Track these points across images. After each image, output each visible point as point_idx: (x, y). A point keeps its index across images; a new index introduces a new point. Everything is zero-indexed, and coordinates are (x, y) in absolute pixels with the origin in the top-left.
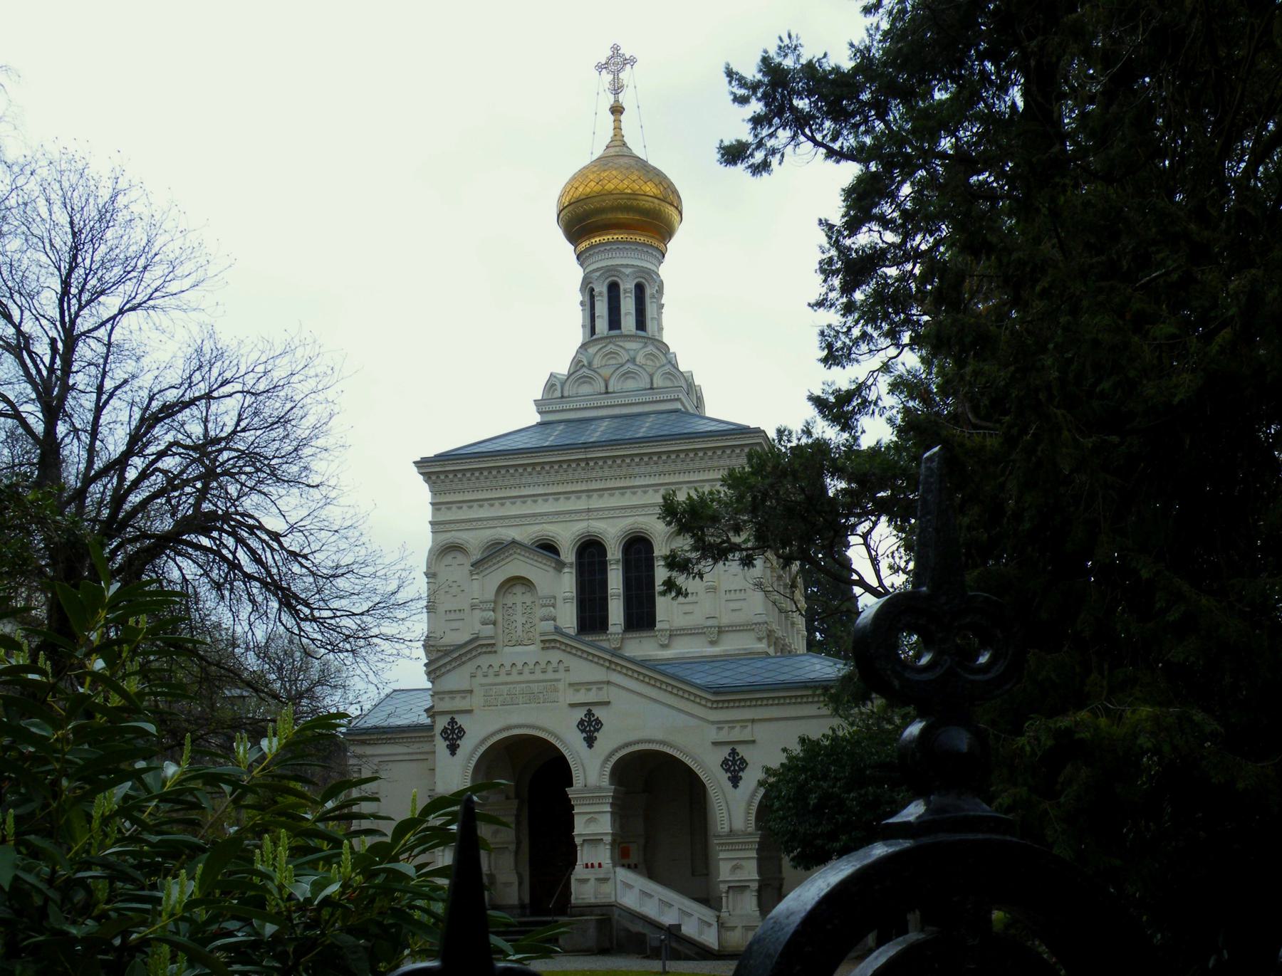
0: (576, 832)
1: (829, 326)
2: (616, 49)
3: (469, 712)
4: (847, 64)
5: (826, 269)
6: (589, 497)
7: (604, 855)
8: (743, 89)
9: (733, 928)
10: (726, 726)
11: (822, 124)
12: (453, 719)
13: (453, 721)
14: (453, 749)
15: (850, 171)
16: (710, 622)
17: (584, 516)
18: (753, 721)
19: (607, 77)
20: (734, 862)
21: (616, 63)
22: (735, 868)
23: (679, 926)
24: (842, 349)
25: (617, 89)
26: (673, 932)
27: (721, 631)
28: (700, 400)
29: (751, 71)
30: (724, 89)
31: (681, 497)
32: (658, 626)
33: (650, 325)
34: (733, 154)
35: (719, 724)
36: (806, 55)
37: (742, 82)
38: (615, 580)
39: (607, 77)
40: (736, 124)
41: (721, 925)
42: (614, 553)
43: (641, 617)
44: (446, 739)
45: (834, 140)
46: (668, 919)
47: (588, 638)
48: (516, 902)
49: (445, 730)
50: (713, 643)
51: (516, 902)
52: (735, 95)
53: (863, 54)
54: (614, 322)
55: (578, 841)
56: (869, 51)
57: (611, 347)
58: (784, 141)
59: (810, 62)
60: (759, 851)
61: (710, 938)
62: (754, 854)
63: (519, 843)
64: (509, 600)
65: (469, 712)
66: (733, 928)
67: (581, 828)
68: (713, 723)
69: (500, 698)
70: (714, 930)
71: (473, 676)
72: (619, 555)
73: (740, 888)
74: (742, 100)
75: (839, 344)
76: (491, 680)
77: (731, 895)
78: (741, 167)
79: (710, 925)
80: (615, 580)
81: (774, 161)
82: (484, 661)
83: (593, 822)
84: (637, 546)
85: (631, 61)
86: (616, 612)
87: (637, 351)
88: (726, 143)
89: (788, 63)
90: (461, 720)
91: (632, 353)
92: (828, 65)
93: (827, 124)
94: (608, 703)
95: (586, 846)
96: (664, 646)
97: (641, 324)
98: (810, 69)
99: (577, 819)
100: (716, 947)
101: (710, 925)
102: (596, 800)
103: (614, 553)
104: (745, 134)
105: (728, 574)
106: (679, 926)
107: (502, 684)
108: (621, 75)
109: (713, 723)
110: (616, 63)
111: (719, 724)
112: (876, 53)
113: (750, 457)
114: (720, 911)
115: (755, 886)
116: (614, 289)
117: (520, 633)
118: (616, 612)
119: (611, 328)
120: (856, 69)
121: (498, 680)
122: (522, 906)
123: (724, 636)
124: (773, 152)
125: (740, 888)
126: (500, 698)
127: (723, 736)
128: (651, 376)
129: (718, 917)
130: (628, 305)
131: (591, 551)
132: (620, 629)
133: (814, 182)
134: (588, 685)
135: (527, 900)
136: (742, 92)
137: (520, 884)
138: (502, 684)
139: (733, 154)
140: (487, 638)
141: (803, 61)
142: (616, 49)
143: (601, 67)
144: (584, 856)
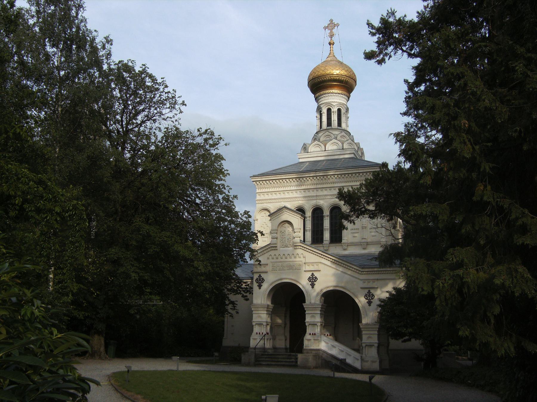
0: (254, 320)
1: (408, 123)
2: (331, 21)
3: (266, 272)
4: (416, 20)
5: (408, 100)
6: (317, 191)
7: (318, 330)
8: (374, 31)
9: (367, 361)
10: (367, 281)
11: (406, 43)
12: (260, 275)
13: (260, 276)
14: (260, 286)
15: (417, 61)
16: (363, 241)
17: (315, 198)
18: (377, 279)
19: (328, 31)
20: (368, 336)
21: (332, 26)
22: (369, 337)
23: (345, 359)
24: (413, 132)
25: (331, 36)
26: (343, 361)
27: (368, 244)
28: (363, 153)
29: (377, 23)
30: (367, 30)
31: (346, 190)
32: (343, 241)
33: (344, 125)
34: (369, 56)
35: (364, 281)
36: (398, 16)
37: (373, 27)
38: (327, 223)
39: (328, 31)
40: (371, 43)
41: (362, 360)
42: (327, 213)
43: (336, 238)
44: (257, 283)
45: (411, 50)
46: (341, 356)
47: (313, 246)
48: (284, 347)
49: (257, 279)
50: (364, 249)
51: (284, 347)
52: (371, 32)
53: (421, 15)
54: (329, 123)
55: (307, 324)
56: (424, 14)
57: (327, 133)
58: (390, 50)
59: (400, 19)
60: (378, 331)
61: (358, 365)
62: (376, 332)
63: (285, 324)
64: (282, 229)
65: (266, 272)
66: (367, 361)
67: (308, 319)
68: (361, 280)
69: (278, 268)
70: (360, 361)
71: (268, 259)
72: (328, 213)
73: (371, 346)
74: (374, 34)
75: (412, 130)
76: (275, 260)
77: (367, 348)
78: (373, 61)
79: (358, 360)
80: (327, 223)
81: (387, 58)
82: (272, 253)
83: (313, 318)
84: (335, 209)
85: (338, 25)
86: (327, 235)
87: (337, 135)
88: (367, 51)
89: (391, 20)
90: (263, 275)
91: (336, 136)
92: (407, 19)
93: (408, 43)
94: (319, 271)
95: (310, 326)
96: (345, 250)
97: (339, 124)
98: (400, 22)
99: (307, 315)
100: (360, 368)
101: (358, 360)
102: (315, 308)
103: (327, 213)
104: (374, 47)
105: (364, 221)
106: (345, 359)
107: (279, 262)
108: (333, 31)
109: (361, 280)
110: (332, 26)
111: (364, 281)
112: (427, 15)
113: (373, 175)
114: (362, 354)
115: (376, 345)
116: (329, 110)
117: (286, 242)
118: (327, 235)
119: (328, 126)
120: (418, 23)
121: (278, 260)
122: (286, 349)
123: (369, 246)
124: (386, 54)
125: (371, 346)
126: (278, 268)
127: (365, 285)
128: (343, 144)
129: (361, 357)
130: (335, 117)
131: (317, 212)
132: (328, 242)
133: (402, 66)
134: (313, 263)
135: (288, 346)
136: (374, 31)
137: (286, 340)
138: (279, 262)
139: (369, 56)
140: (273, 244)
141: (397, 19)
142: (331, 21)
143: (325, 28)
144: (309, 330)
